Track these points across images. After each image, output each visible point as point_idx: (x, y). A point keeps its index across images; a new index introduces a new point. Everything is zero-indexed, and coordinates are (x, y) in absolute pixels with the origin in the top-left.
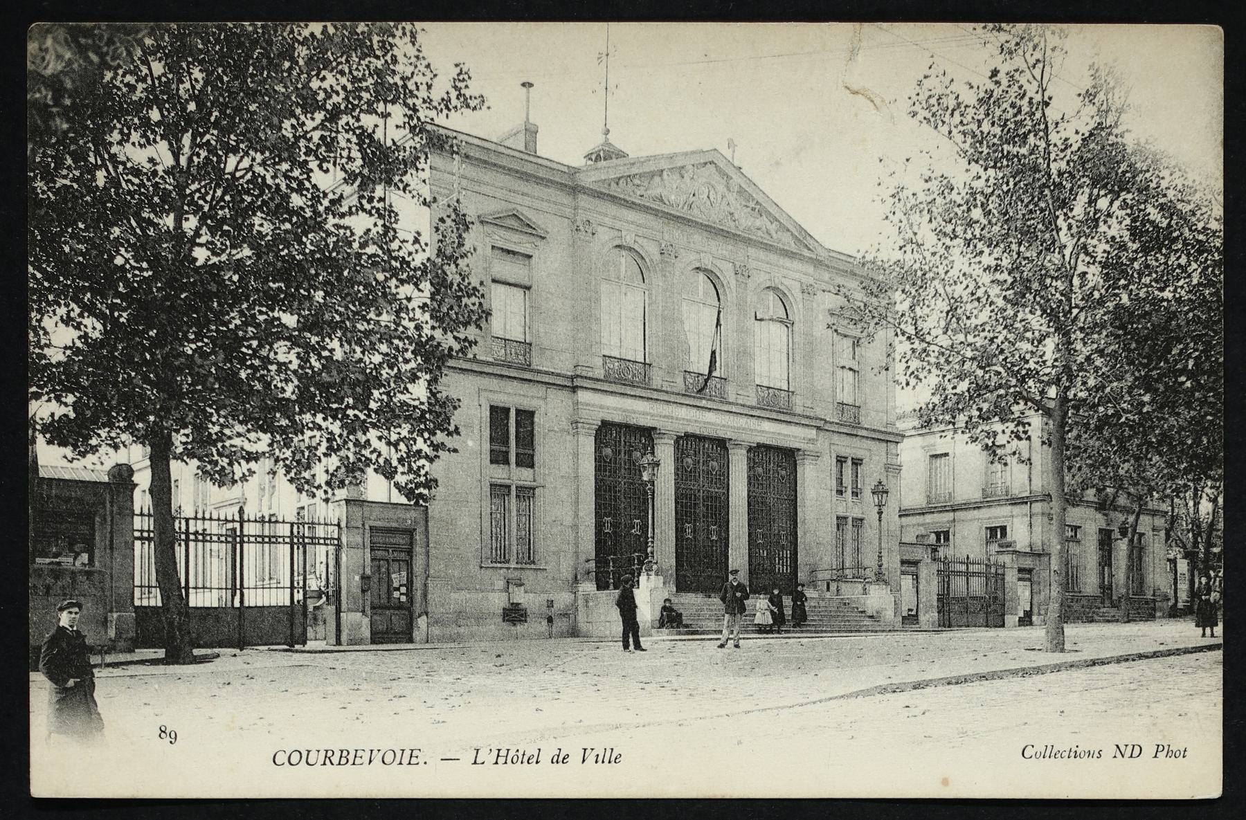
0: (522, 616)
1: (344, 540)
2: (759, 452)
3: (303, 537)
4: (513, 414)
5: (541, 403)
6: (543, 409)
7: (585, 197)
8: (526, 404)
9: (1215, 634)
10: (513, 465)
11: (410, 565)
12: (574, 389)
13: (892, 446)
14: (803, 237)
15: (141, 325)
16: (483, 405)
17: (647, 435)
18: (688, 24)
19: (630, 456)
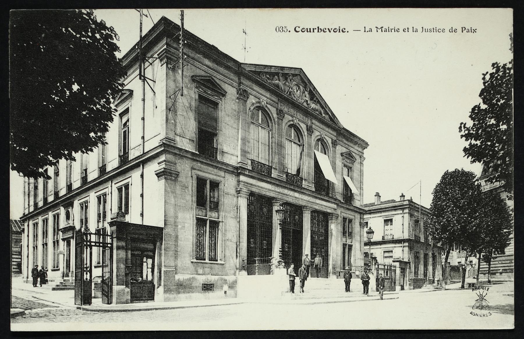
0: (205, 287)
1: (115, 245)
2: (315, 213)
3: (90, 242)
4: (208, 182)
5: (222, 179)
6: (223, 182)
7: (242, 198)
8: (351, 217)
9: (223, 176)
10: (208, 209)
11: (153, 258)
12: (238, 175)
13: (362, 215)
14: (333, 118)
15: (77, 130)
16: (194, 176)
17: (269, 201)
18: (302, 9)
19: (289, 250)
